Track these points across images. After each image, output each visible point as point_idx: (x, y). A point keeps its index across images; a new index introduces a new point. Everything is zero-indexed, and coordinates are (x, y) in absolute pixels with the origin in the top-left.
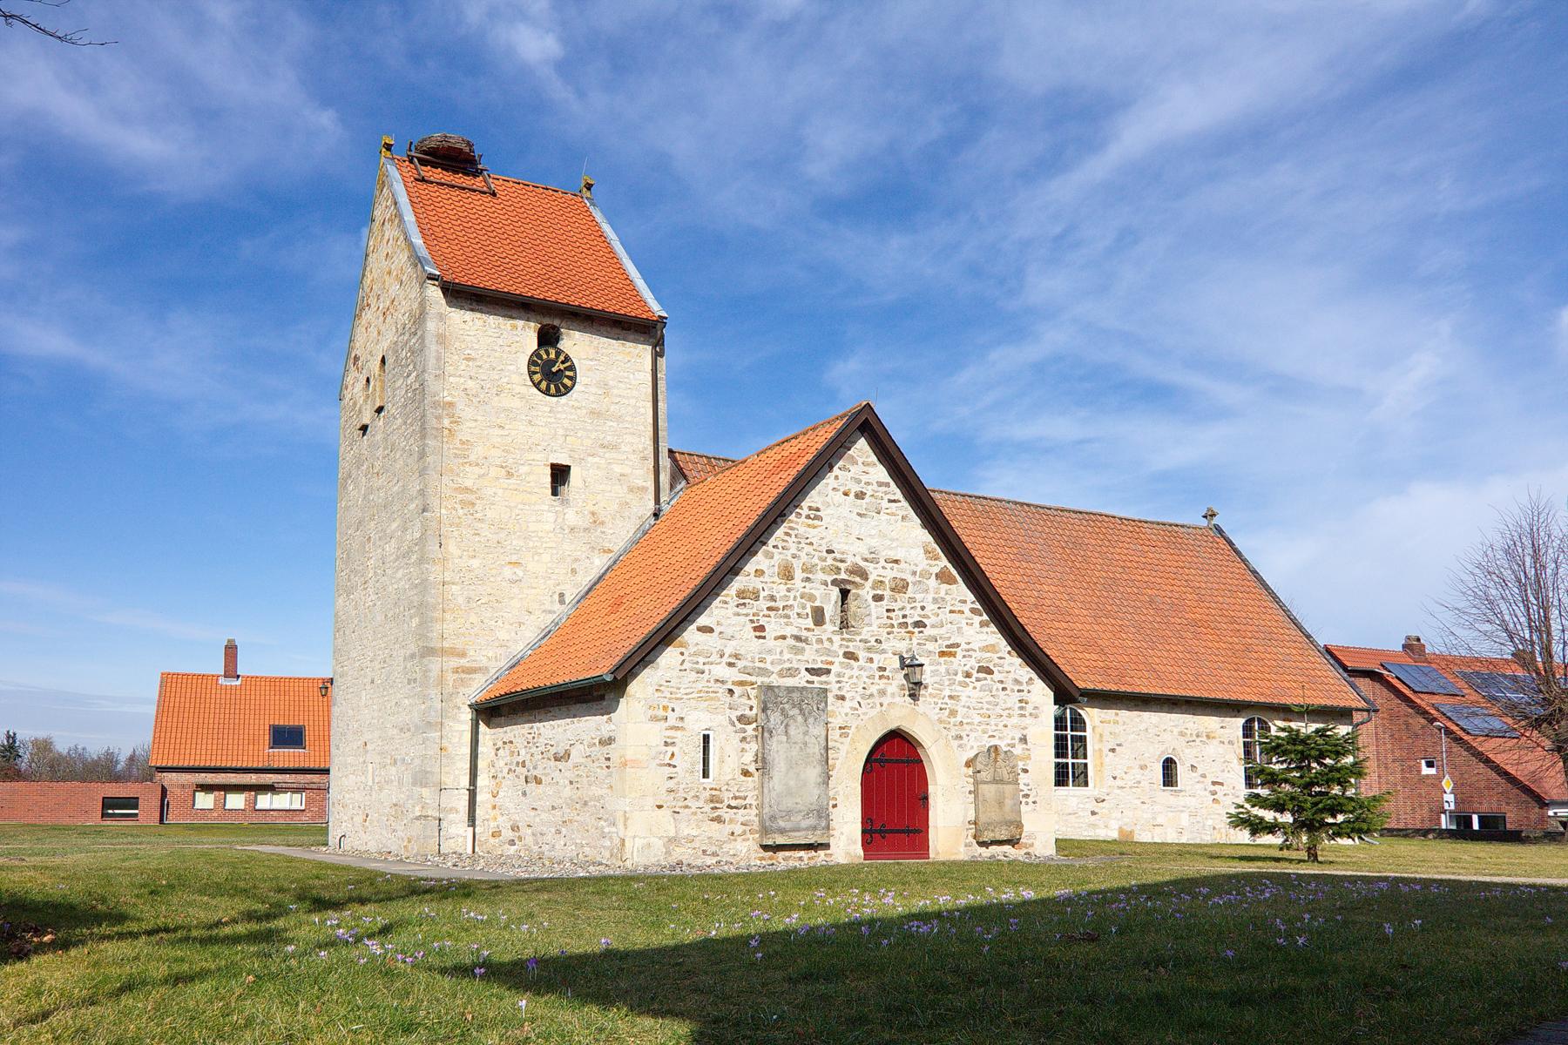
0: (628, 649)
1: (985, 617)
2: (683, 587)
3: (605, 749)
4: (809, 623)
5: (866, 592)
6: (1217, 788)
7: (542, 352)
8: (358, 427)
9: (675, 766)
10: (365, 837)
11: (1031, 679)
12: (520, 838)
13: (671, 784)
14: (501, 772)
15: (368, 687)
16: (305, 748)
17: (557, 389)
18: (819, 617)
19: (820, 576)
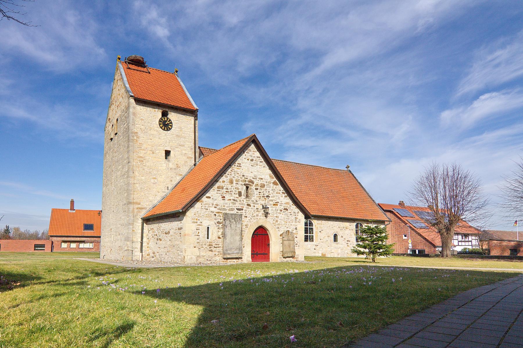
1: (286, 195)
3: (180, 231)
4: (237, 196)
5: (253, 187)
6: (348, 242)
7: (163, 118)
9: (199, 236)
11: (298, 212)
12: (155, 256)
13: (198, 241)
14: (150, 237)
16: (93, 230)
17: (167, 129)
18: (240, 194)
19: (241, 183)
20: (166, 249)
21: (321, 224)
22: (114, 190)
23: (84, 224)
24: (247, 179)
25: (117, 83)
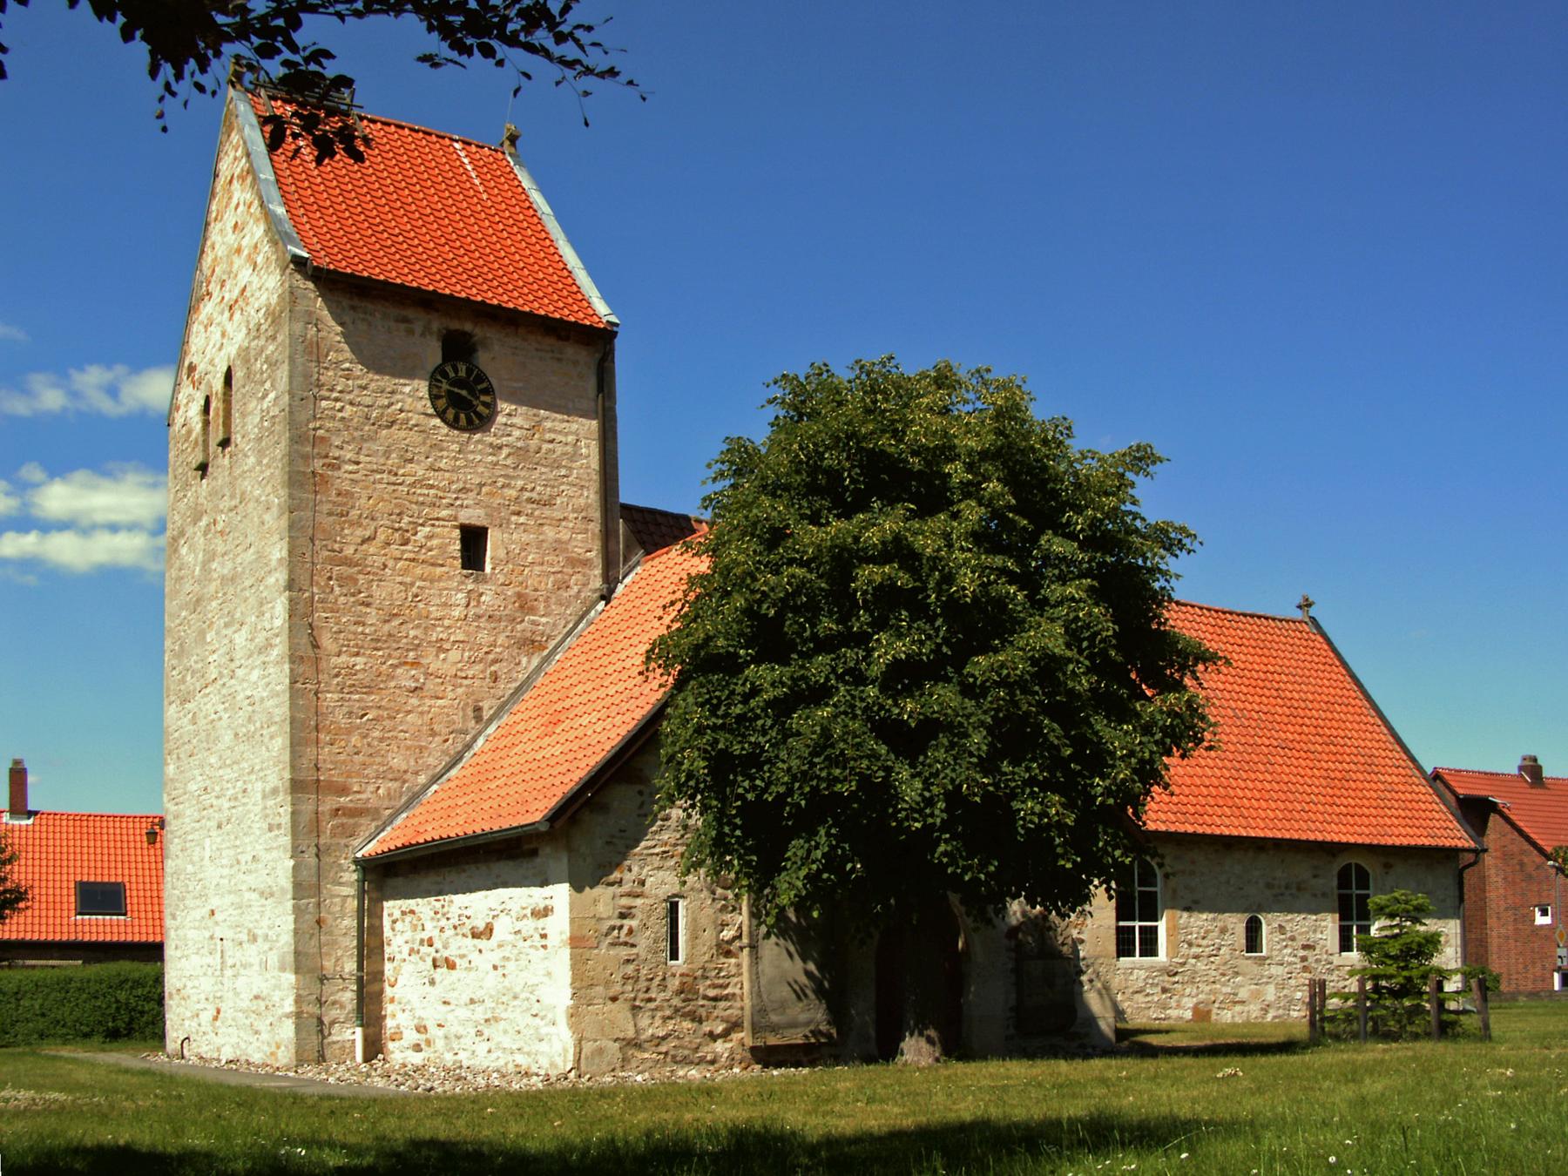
0: (569, 787)
2: (642, 701)
3: (542, 922)
7: (449, 369)
8: (194, 466)
9: (633, 946)
10: (218, 1041)
12: (428, 1043)
14: (400, 952)
15: (214, 833)
16: (125, 914)
17: (470, 421)
20: (479, 1009)
21: (1192, 873)
22: (220, 719)
23: (82, 883)
25: (229, 191)
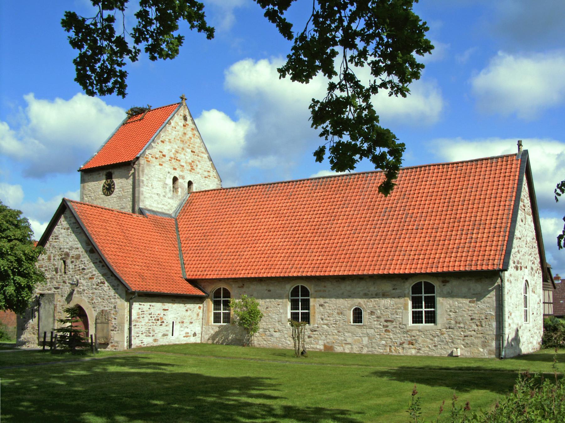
4: (54, 273)
6: (389, 324)
11: (118, 284)
24: (63, 252)
